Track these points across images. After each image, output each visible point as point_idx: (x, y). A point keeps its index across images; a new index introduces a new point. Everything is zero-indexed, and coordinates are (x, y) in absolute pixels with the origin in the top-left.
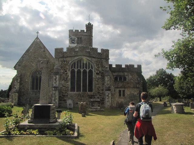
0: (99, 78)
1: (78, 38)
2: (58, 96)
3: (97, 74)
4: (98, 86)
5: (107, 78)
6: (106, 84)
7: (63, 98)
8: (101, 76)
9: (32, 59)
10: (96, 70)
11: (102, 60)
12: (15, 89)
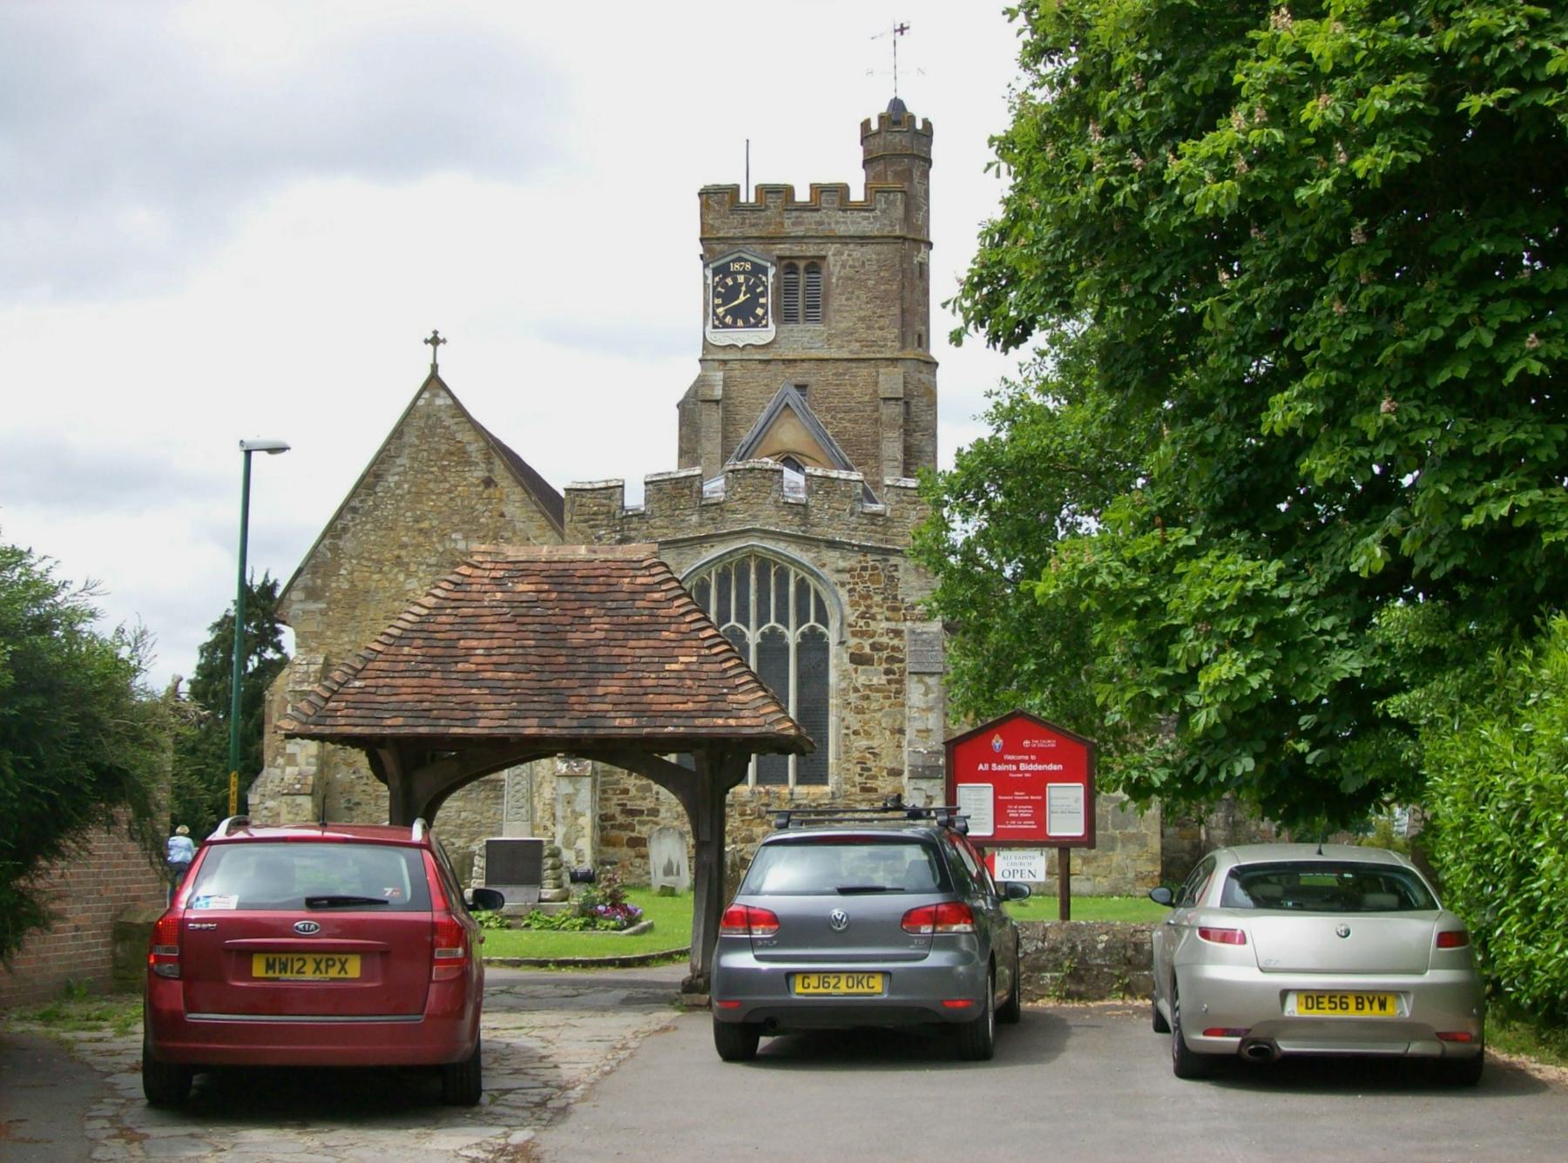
0: (869, 687)
1: (788, 266)
2: (589, 814)
3: (858, 659)
4: (863, 743)
5: (922, 689)
6: (910, 733)
7: (622, 827)
8: (888, 672)
9: (403, 546)
10: (847, 631)
11: (894, 560)
12: (289, 770)
